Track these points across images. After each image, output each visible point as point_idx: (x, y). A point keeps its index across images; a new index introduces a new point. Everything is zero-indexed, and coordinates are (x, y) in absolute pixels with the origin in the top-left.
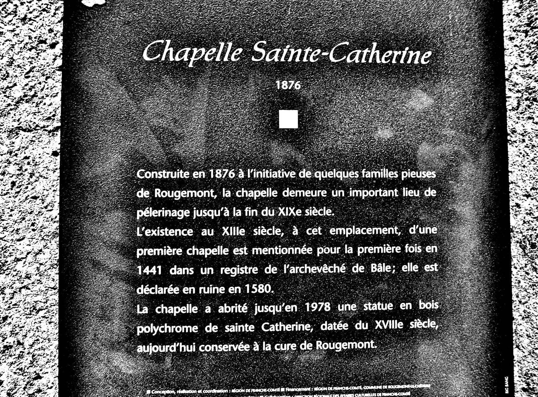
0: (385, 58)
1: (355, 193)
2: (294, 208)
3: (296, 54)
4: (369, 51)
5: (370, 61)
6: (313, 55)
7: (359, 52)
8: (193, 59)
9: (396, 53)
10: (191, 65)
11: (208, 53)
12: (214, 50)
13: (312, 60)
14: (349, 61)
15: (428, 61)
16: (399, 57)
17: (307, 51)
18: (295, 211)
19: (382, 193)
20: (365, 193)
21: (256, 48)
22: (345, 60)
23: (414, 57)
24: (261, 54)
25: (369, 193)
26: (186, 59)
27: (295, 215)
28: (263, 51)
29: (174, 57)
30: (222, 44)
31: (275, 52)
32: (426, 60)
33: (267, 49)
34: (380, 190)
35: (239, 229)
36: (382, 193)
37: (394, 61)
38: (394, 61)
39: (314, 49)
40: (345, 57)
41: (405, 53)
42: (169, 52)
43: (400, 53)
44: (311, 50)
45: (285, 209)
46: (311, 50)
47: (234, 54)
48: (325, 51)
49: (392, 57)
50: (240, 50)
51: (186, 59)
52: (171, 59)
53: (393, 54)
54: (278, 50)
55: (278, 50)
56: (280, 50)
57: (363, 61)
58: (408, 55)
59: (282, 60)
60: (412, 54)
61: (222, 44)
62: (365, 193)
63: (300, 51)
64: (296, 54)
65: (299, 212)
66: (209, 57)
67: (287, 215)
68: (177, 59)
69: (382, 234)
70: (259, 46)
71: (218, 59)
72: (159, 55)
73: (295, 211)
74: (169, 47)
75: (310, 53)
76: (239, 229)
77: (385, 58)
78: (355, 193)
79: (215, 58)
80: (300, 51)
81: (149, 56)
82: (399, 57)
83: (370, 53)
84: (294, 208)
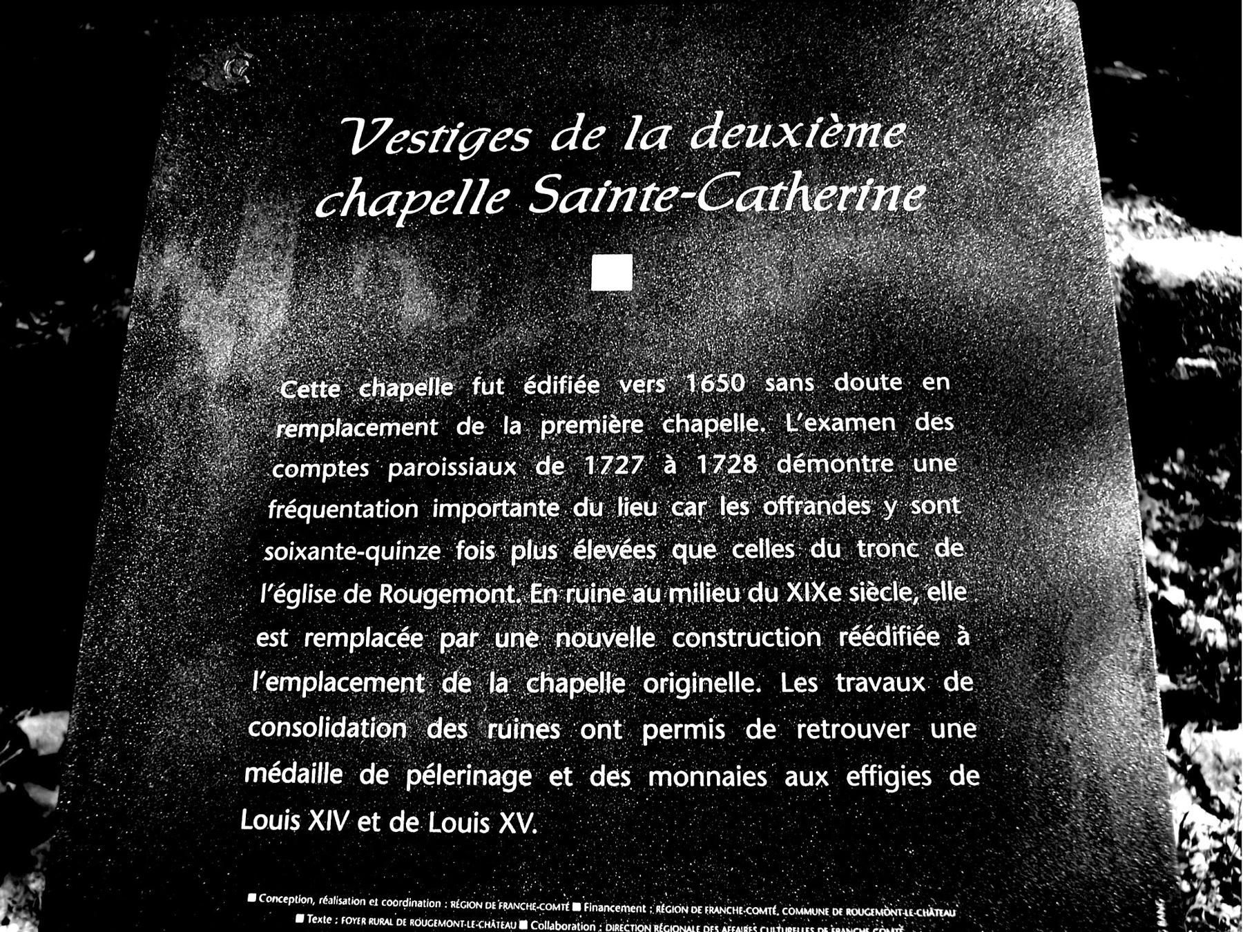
0: (822, 201)
1: (446, 509)
2: (823, 584)
3: (624, 198)
4: (786, 188)
5: (788, 207)
6: (661, 198)
7: (763, 189)
8: (405, 211)
9: (846, 190)
10: (400, 224)
11: (437, 200)
12: (451, 193)
13: (658, 207)
14: (740, 207)
15: (671, 206)
16: (853, 198)
17: (649, 190)
18: (826, 592)
19: (509, 509)
20: (469, 510)
21: (539, 188)
22: (733, 206)
23: (888, 197)
24: (550, 199)
25: (477, 510)
26: (391, 213)
27: (825, 599)
28: (554, 194)
29: (366, 209)
30: (469, 183)
31: (757, 192)
32: (664, 204)
33: (562, 189)
34: (505, 504)
35: (643, 632)
36: (509, 509)
37: (841, 207)
38: (841, 207)
39: (663, 185)
40: (732, 201)
41: (865, 190)
42: (356, 200)
43: (854, 189)
44: (658, 189)
45: (803, 586)
46: (658, 189)
47: (493, 200)
48: (687, 190)
49: (835, 200)
50: (506, 193)
51: (391, 213)
52: (361, 212)
53: (840, 192)
54: (587, 191)
55: (587, 191)
56: (590, 190)
57: (773, 207)
58: (872, 195)
59: (595, 209)
60: (618, 192)
61: (469, 183)
62: (469, 510)
63: (633, 191)
64: (624, 198)
65: (835, 593)
66: (440, 207)
67: (807, 599)
68: (373, 212)
69: (642, 646)
70: (546, 184)
71: (457, 211)
72: (732, 201)
73: (826, 592)
74: (801, 184)
75: (654, 195)
76: (643, 632)
77: (822, 201)
78: (446, 509)
79: (835, 207)
80: (633, 191)
81: (710, 203)
82: (853, 198)
83: (788, 192)
84: (823, 584)
